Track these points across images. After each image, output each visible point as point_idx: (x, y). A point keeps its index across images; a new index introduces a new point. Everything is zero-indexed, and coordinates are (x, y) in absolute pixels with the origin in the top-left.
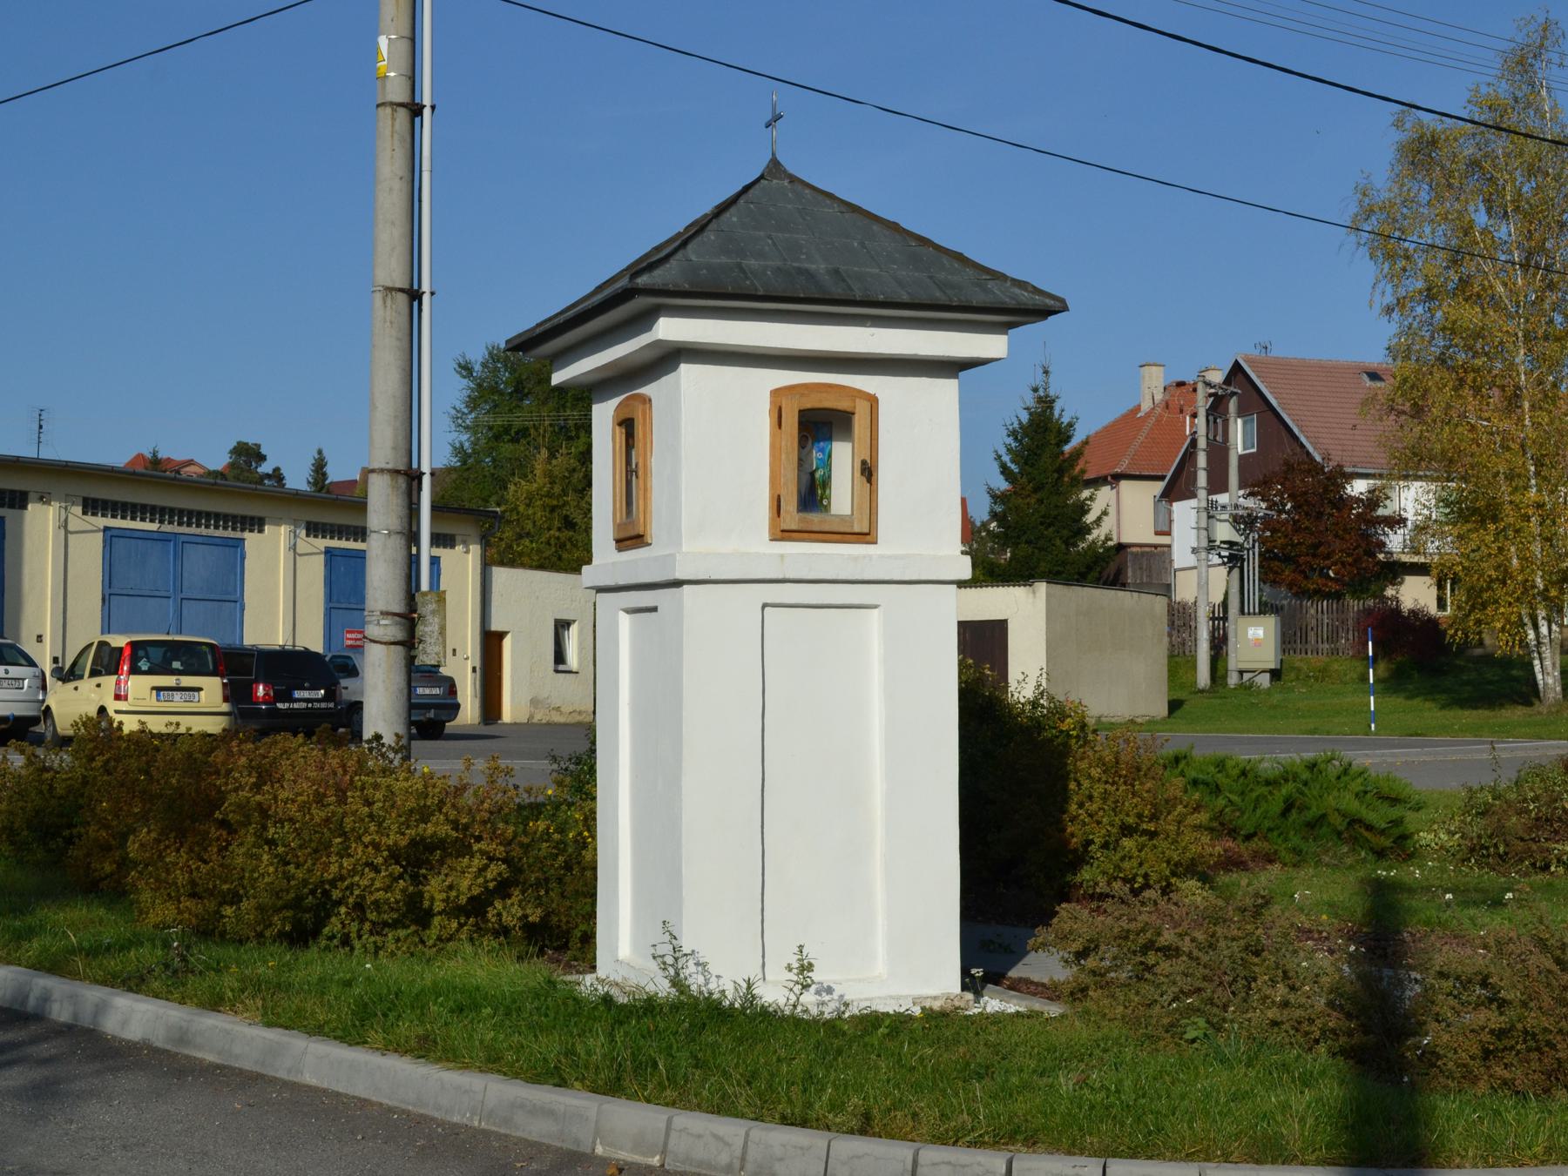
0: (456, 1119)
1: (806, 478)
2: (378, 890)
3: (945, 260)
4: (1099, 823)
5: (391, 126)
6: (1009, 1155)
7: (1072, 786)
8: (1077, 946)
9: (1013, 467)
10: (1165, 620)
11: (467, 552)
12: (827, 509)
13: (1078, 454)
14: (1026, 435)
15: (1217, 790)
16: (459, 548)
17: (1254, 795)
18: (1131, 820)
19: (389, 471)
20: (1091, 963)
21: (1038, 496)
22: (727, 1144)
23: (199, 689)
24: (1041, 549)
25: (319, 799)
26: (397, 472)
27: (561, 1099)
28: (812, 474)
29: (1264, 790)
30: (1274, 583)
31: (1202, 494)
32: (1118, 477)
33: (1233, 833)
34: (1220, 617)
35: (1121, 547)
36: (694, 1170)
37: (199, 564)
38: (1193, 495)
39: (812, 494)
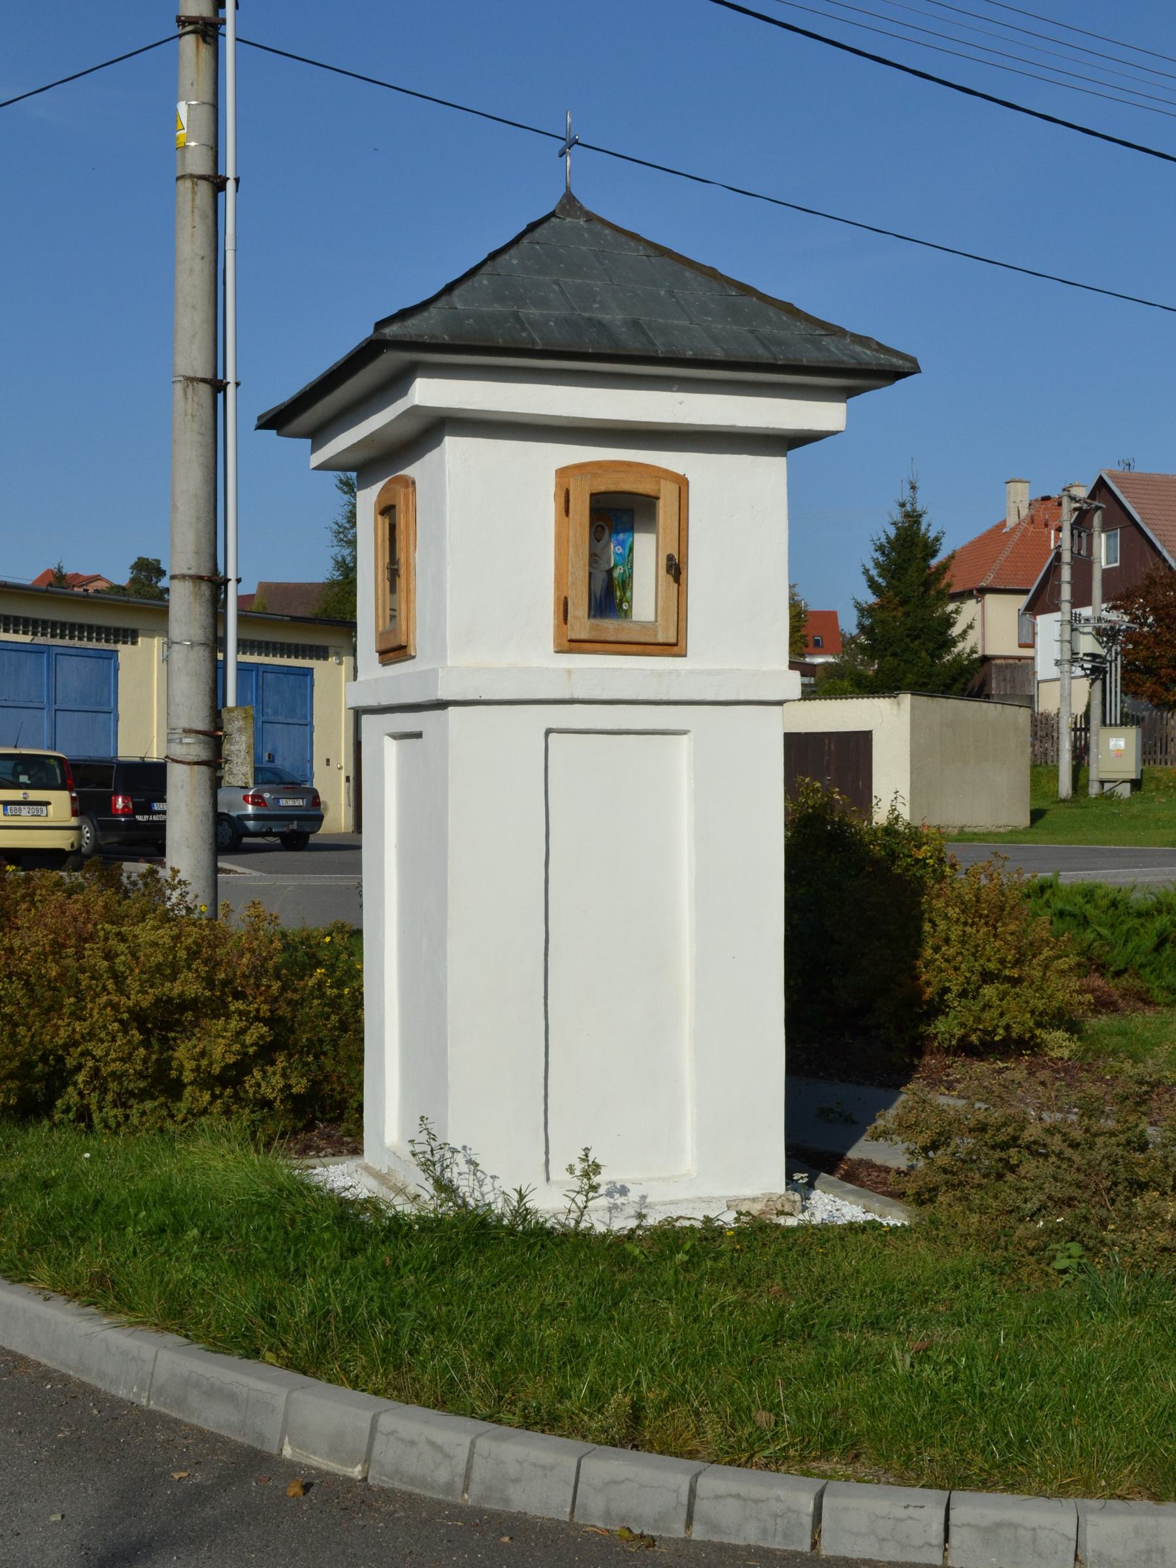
0: (121, 1393)
1: (601, 577)
2: (114, 1061)
3: (771, 312)
4: (956, 969)
5: (190, 201)
6: (818, 1483)
7: (927, 927)
8: (925, 1138)
9: (880, 580)
10: (1029, 732)
11: (340, 663)
12: (627, 614)
13: (944, 568)
14: (893, 549)
15: (1085, 922)
16: (333, 660)
17: (1125, 928)
18: (992, 966)
19: (192, 577)
20: (941, 1157)
21: (905, 609)
22: (447, 1456)
23: (47, 803)
24: (906, 661)
25: (57, 948)
26: (201, 578)
27: (244, 1379)
28: (610, 572)
29: (1137, 922)
30: (1135, 694)
31: (1066, 607)
32: (983, 591)
33: (1102, 969)
34: (1082, 728)
35: (986, 659)
36: (403, 1487)
37: (73, 676)
38: (1057, 609)
39: (608, 596)
